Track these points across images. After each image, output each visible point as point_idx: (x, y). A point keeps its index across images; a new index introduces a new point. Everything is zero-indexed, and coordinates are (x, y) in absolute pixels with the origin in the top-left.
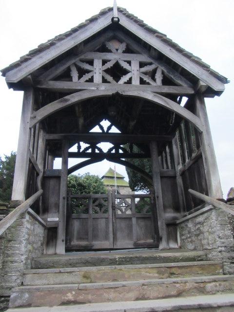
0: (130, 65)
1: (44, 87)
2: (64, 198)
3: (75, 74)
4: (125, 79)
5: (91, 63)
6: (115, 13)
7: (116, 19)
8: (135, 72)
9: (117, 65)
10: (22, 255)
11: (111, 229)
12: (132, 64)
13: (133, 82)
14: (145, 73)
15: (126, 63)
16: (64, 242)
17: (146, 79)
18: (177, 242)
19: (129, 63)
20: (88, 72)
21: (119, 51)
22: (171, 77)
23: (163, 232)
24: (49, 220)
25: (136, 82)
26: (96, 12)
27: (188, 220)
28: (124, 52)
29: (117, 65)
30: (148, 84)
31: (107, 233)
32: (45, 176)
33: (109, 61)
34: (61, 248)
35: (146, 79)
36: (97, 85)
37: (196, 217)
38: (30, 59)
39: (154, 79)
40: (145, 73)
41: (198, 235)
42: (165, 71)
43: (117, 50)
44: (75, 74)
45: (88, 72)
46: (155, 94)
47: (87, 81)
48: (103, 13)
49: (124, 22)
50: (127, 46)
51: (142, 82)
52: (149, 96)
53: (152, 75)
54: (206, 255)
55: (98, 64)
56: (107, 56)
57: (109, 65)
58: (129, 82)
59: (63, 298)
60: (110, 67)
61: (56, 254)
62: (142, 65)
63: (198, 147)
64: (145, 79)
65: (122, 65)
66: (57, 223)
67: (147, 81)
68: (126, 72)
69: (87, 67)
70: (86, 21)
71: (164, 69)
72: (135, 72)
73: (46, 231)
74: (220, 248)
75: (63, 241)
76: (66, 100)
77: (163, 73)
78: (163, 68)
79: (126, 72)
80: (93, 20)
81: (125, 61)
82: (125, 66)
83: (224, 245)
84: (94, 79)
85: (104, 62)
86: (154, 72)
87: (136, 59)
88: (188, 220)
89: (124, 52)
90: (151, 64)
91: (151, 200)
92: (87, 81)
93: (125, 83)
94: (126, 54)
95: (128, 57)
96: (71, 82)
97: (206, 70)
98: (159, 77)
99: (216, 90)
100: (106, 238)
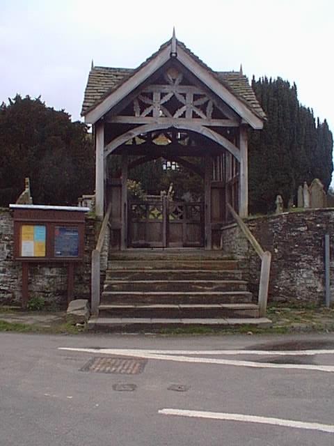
1: (113, 122)
3: (137, 109)
6: (174, 47)
7: (174, 55)
8: (189, 106)
11: (164, 232)
14: (197, 107)
17: (199, 113)
18: (220, 245)
19: (184, 95)
21: (177, 82)
23: (208, 235)
28: (180, 84)
31: (161, 235)
35: (199, 113)
36: (154, 120)
38: (102, 102)
42: (216, 104)
43: (174, 80)
44: (137, 109)
47: (147, 116)
48: (163, 48)
49: (182, 58)
55: (156, 96)
56: (167, 89)
59: (27, 180)
62: (196, 97)
64: (197, 113)
67: (199, 114)
69: (147, 101)
72: (189, 106)
74: (307, 241)
76: (131, 134)
77: (214, 106)
78: (214, 101)
81: (181, 94)
82: (181, 99)
86: (206, 104)
89: (180, 84)
90: (204, 96)
91: (200, 208)
92: (147, 116)
93: (180, 117)
94: (181, 87)
95: (185, 89)
96: (133, 117)
98: (209, 109)
100: (160, 240)
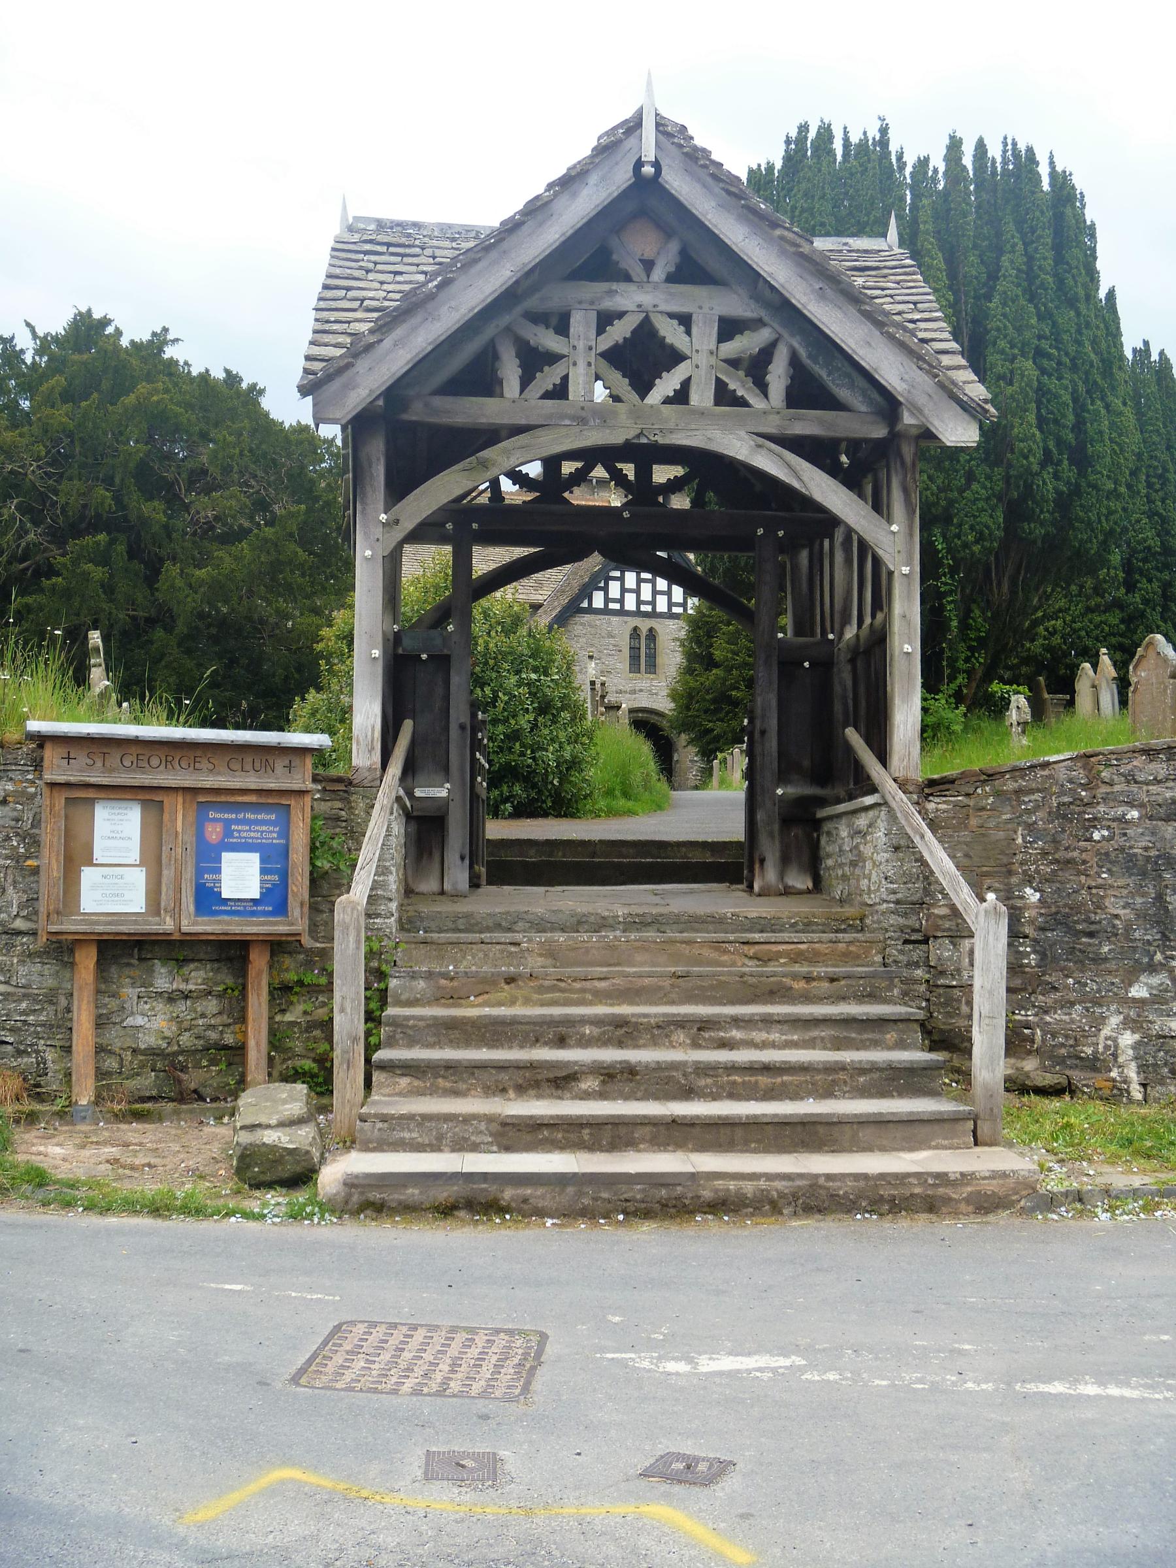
0: (688, 332)
2: (462, 727)
3: (510, 372)
4: (667, 384)
5: (562, 327)
8: (701, 357)
9: (645, 332)
10: (391, 900)
12: (694, 330)
13: (694, 398)
15: (675, 322)
16: (467, 861)
17: (738, 385)
19: (685, 320)
20: (553, 358)
21: (658, 274)
22: (820, 376)
24: (418, 793)
25: (702, 396)
26: (583, 149)
27: (839, 816)
28: (671, 279)
29: (645, 332)
30: (742, 403)
32: (400, 651)
33: (621, 315)
34: (458, 875)
35: (738, 385)
37: (855, 812)
39: (763, 388)
40: (734, 363)
41: (853, 864)
42: (803, 353)
43: (649, 265)
44: (510, 372)
45: (553, 358)
46: (761, 440)
48: (607, 149)
50: (684, 253)
51: (724, 396)
52: (737, 444)
53: (756, 368)
54: (861, 920)
55: (581, 324)
57: (619, 332)
58: (681, 397)
60: (621, 341)
61: (442, 893)
62: (729, 328)
63: (877, 605)
65: (662, 333)
66: (446, 802)
68: (676, 357)
69: (549, 341)
70: (550, 186)
71: (796, 345)
72: (701, 357)
73: (413, 828)
75: (462, 858)
77: (794, 361)
79: (676, 357)
80: (568, 182)
81: (671, 316)
82: (671, 333)
83: (892, 897)
84: (571, 389)
85: (605, 320)
86: (765, 356)
87: (707, 305)
88: (839, 816)
89: (671, 279)
92: (547, 396)
97: (928, 372)
98: (778, 376)
99: (948, 444)
